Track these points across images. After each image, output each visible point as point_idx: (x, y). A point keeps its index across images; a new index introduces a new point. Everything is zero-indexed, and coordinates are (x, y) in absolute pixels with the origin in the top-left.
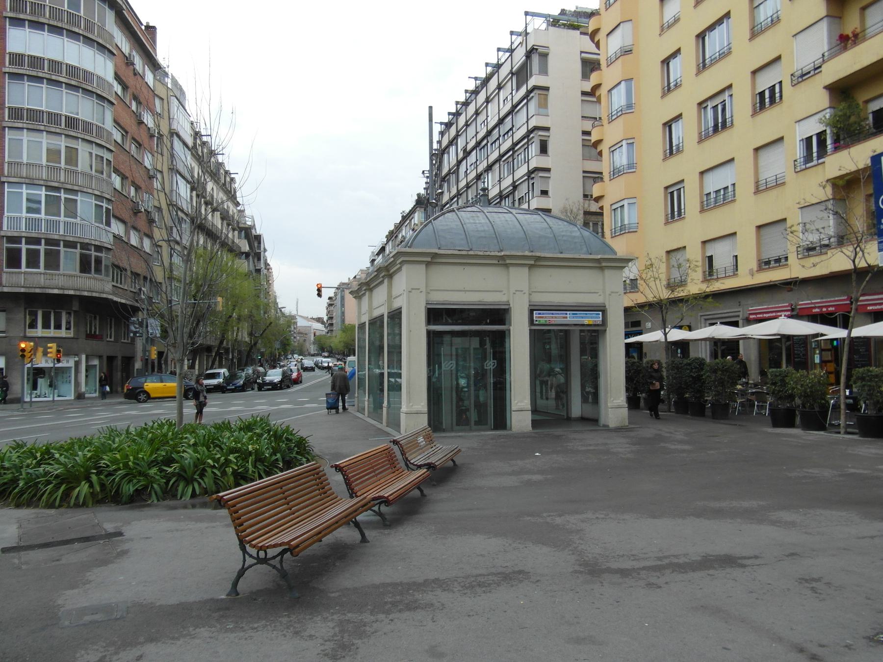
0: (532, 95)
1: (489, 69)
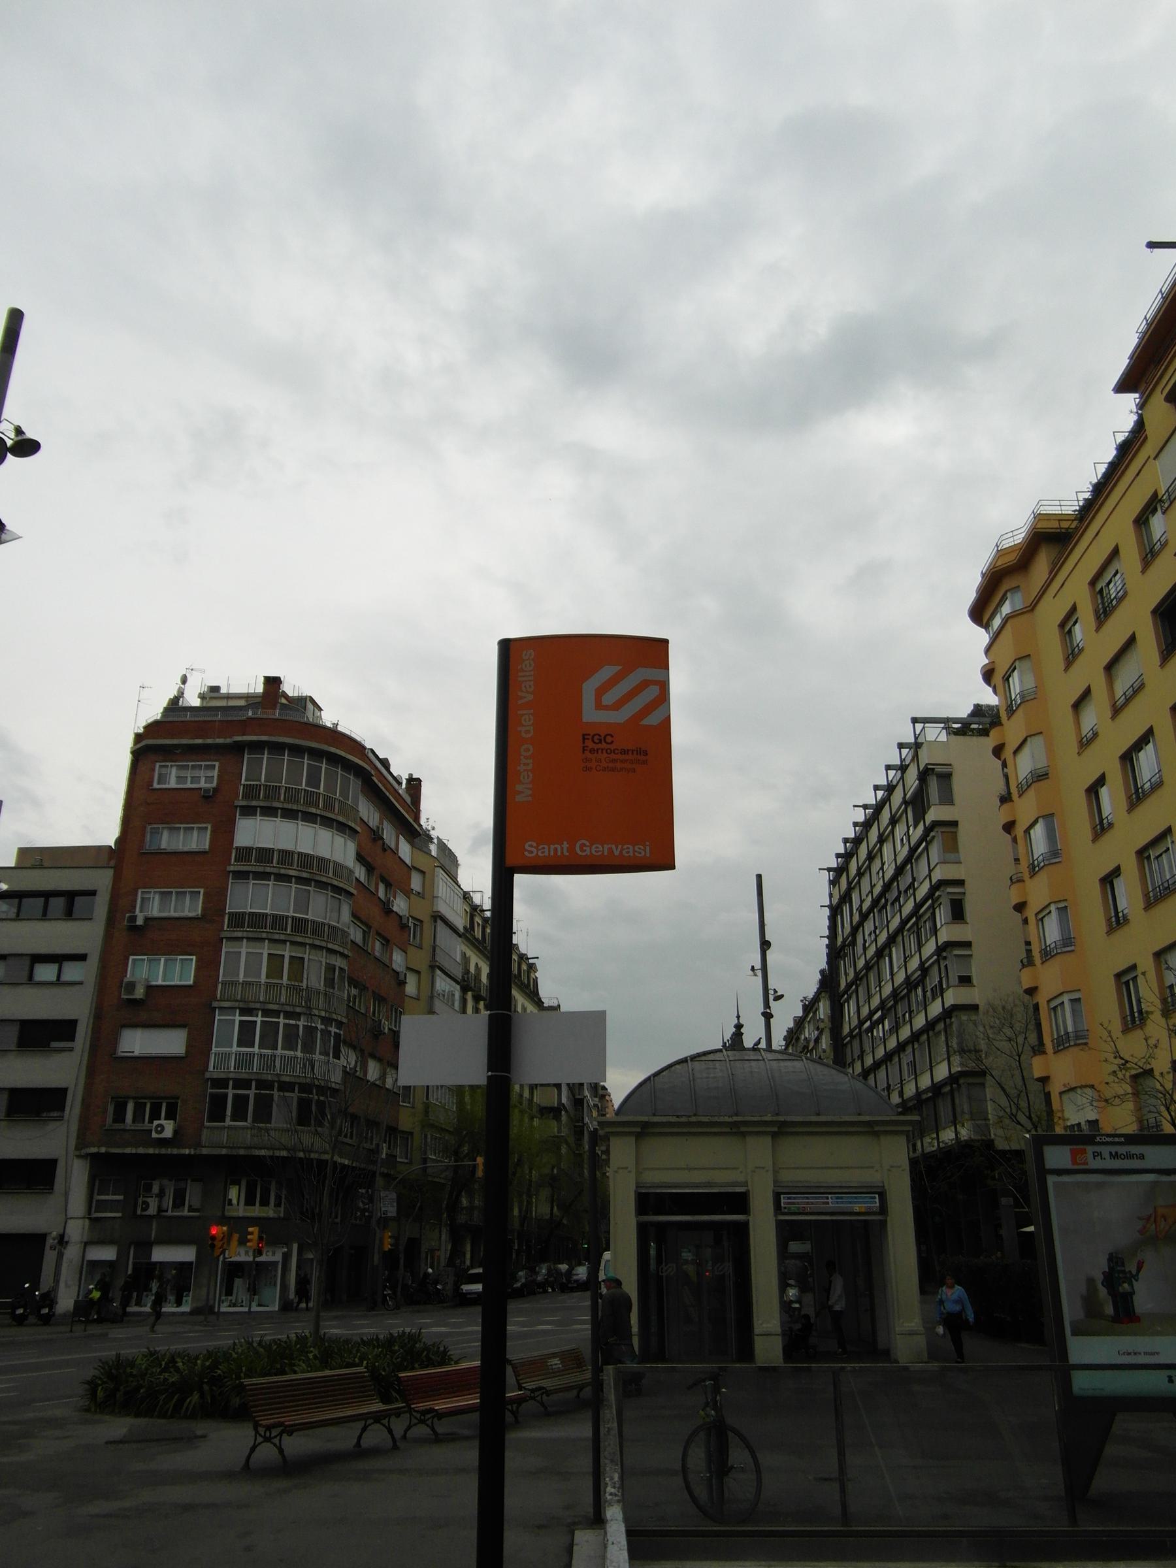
0: (932, 834)
1: (880, 794)
